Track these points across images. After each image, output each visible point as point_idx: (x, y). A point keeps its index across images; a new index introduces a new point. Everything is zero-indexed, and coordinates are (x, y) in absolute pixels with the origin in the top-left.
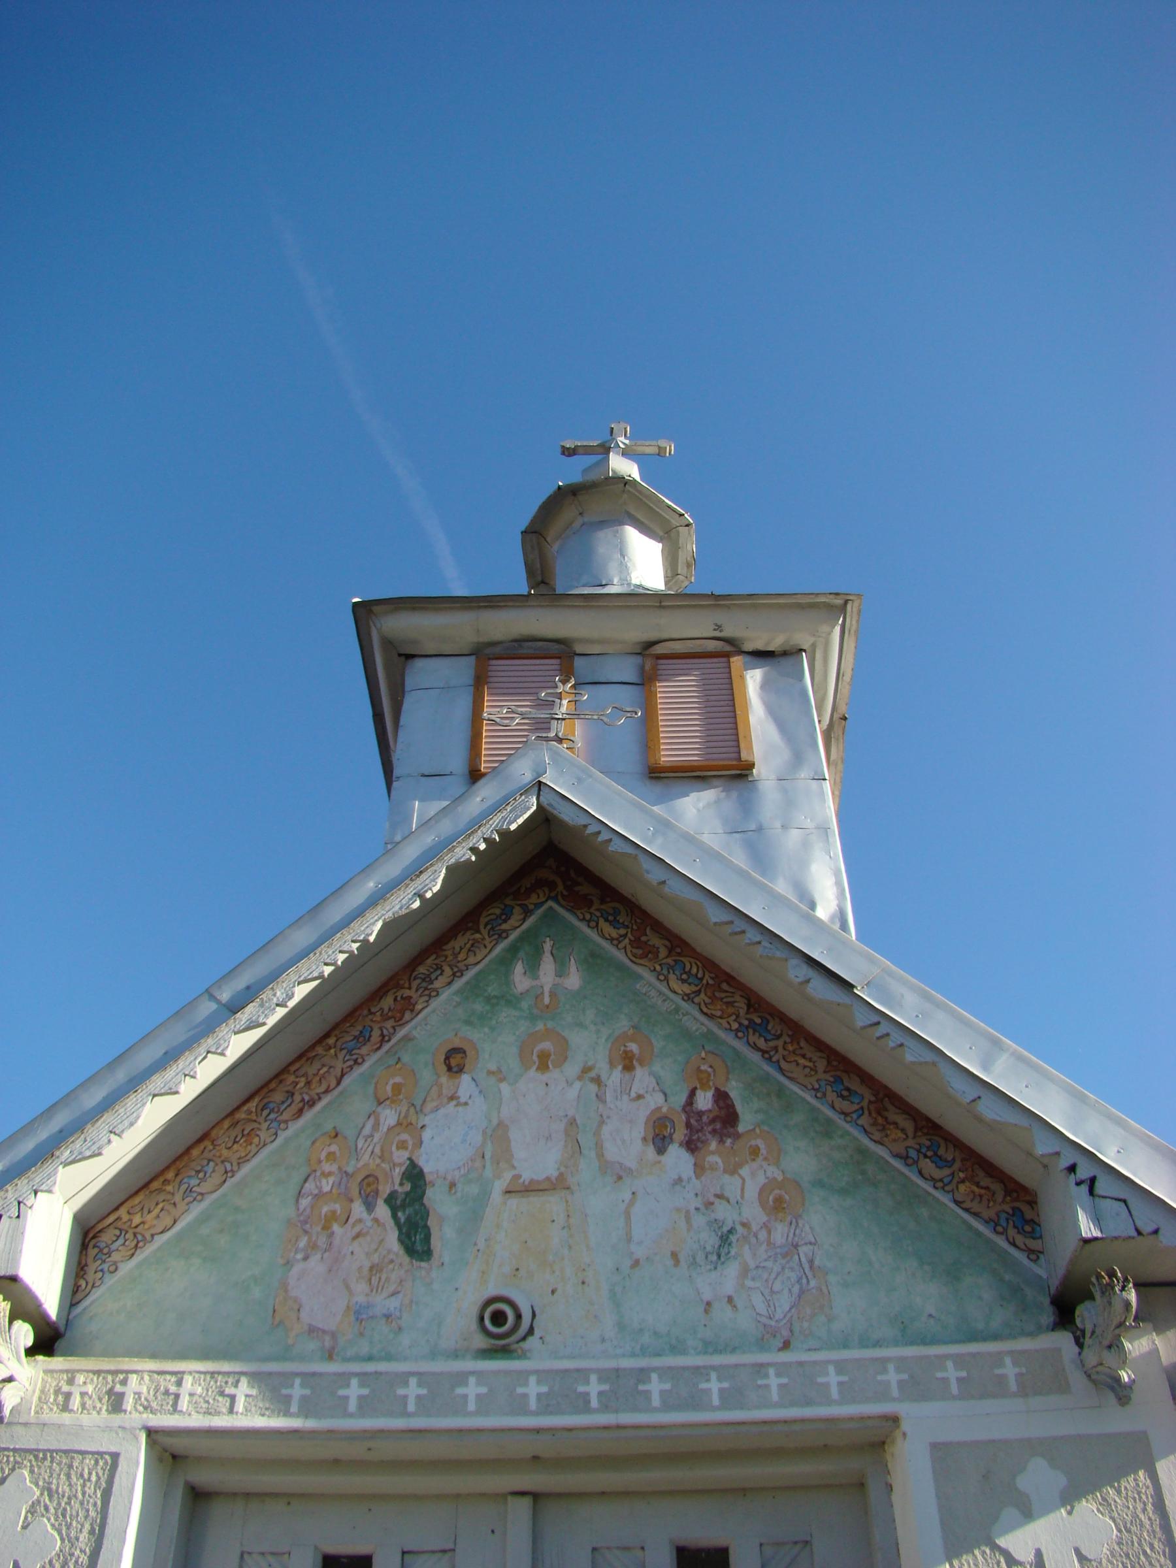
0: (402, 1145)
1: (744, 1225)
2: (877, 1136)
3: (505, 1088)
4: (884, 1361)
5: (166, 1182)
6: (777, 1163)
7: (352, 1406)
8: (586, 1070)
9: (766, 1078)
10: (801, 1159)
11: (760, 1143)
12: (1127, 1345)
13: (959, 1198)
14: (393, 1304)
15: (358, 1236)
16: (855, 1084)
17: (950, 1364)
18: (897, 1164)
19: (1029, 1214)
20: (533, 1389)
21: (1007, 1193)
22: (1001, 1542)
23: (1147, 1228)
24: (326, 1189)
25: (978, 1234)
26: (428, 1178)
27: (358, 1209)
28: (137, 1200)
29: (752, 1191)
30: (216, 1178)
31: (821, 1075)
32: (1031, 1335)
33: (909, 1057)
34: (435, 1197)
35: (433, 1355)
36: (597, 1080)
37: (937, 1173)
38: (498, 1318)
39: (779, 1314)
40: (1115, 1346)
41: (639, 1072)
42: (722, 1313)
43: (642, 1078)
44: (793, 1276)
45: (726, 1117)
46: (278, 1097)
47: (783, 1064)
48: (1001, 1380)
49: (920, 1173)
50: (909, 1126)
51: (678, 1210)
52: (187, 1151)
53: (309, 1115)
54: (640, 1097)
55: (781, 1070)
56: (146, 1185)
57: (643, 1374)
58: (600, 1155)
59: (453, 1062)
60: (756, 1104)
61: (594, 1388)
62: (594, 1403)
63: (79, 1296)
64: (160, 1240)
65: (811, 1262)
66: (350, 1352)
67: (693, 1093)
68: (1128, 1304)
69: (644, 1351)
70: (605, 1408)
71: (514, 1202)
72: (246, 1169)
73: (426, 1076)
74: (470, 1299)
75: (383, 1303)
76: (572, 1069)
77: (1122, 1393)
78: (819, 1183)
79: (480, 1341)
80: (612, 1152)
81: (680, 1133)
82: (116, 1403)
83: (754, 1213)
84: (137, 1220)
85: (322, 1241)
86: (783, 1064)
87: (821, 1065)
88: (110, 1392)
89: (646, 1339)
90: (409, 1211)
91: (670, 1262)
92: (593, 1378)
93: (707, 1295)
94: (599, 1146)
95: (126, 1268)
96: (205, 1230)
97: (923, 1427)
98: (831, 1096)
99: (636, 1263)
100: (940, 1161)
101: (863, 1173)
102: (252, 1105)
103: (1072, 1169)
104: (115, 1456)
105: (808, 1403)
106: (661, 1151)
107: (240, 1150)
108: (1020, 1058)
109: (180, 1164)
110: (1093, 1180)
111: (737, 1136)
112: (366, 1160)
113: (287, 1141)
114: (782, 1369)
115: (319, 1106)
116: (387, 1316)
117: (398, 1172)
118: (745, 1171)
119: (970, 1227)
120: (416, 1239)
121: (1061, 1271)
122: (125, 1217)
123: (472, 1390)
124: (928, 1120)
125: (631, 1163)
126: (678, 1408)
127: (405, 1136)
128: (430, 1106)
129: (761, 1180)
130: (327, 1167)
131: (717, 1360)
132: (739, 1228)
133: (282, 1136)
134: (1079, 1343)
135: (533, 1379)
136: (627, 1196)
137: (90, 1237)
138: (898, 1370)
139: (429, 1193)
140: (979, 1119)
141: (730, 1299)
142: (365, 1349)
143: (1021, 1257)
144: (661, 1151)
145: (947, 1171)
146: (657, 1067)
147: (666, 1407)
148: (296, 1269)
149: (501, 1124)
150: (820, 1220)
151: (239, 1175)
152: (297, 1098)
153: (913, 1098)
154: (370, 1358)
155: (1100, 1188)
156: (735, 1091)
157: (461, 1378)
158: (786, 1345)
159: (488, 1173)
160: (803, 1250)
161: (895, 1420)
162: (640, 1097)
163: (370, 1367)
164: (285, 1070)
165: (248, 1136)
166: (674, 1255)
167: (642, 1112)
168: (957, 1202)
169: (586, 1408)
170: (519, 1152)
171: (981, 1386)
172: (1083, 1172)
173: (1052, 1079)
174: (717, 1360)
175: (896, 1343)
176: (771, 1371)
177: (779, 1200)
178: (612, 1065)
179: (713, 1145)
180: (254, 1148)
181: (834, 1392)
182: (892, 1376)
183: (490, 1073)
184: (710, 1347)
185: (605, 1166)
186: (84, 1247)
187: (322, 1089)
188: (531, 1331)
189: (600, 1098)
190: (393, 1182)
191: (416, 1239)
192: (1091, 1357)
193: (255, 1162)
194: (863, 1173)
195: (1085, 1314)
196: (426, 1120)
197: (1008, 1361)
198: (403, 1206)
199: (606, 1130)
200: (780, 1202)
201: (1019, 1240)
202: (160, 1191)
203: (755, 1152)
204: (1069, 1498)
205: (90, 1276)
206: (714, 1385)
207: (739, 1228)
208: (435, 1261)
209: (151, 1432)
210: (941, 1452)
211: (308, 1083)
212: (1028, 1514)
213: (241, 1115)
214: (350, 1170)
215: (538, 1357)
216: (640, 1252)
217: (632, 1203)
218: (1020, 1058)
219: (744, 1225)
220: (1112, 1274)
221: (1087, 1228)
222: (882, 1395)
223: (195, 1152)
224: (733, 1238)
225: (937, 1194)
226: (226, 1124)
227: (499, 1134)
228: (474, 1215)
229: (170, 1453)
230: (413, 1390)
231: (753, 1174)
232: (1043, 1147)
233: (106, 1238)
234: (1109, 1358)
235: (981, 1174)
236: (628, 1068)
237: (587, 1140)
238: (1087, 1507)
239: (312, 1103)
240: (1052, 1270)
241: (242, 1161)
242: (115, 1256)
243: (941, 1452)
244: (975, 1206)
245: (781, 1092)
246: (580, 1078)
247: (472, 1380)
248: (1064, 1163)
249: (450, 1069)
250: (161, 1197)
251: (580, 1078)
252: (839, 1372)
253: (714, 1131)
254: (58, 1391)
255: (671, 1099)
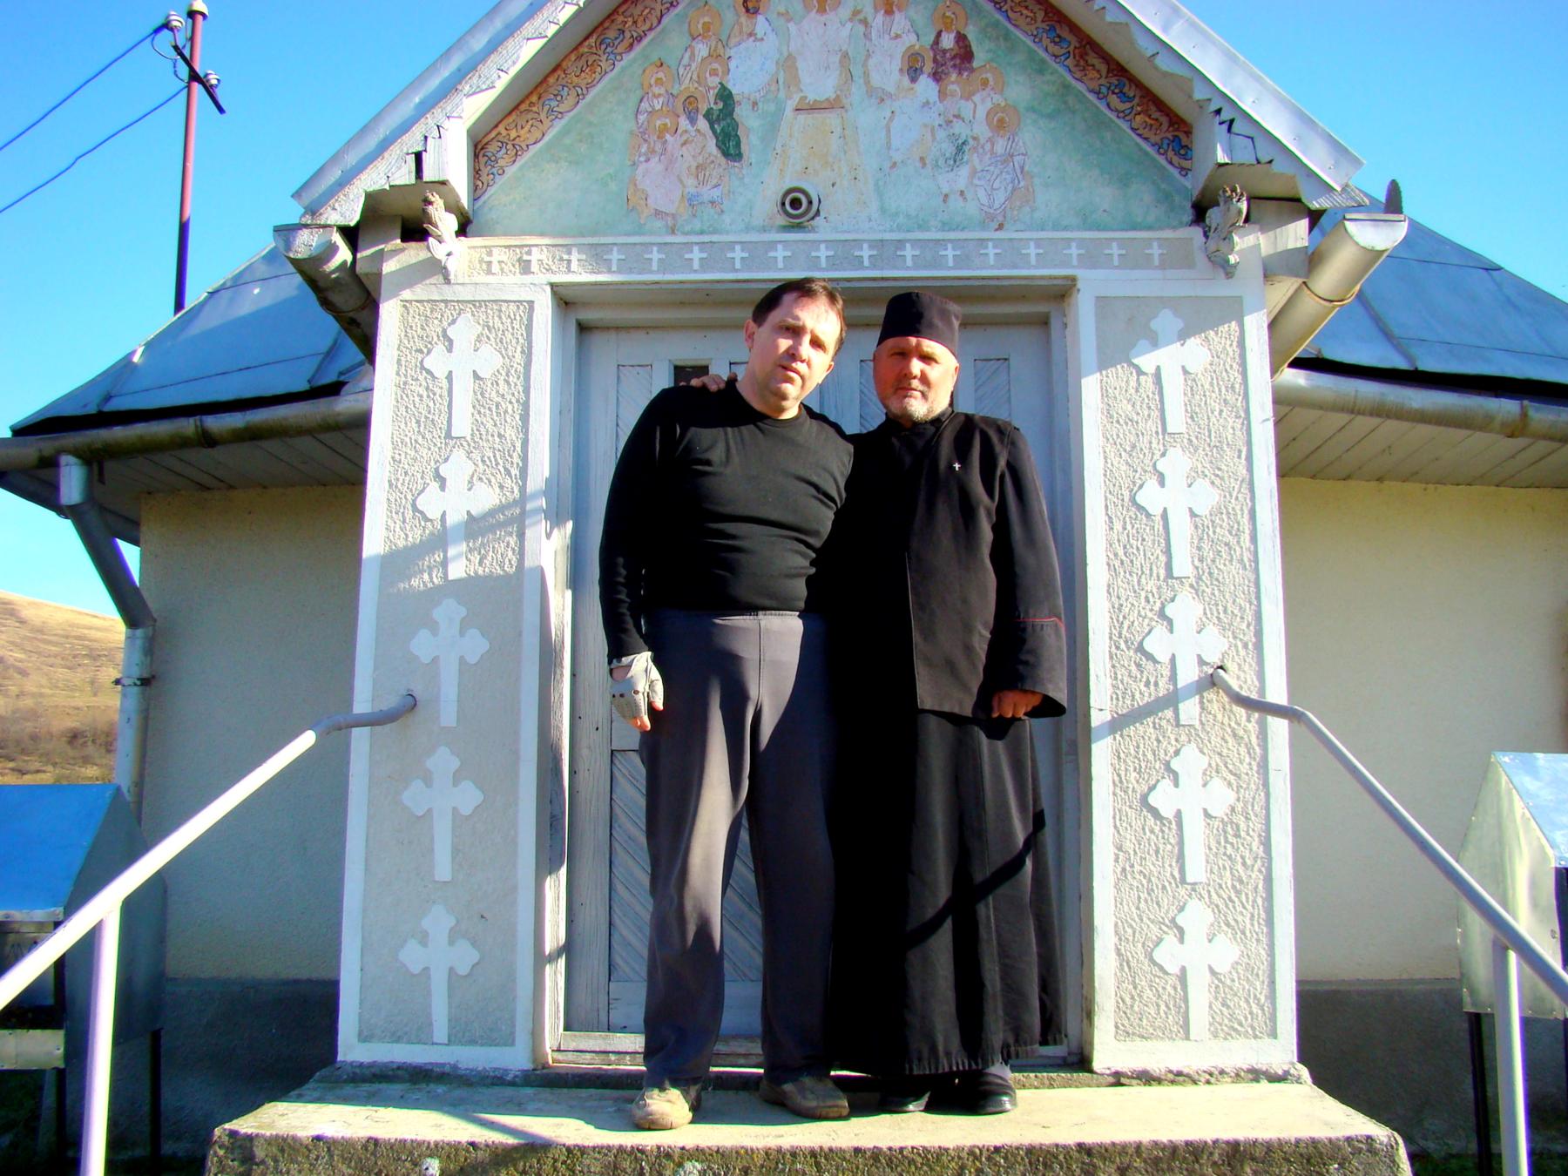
0: (714, 73)
1: (975, 139)
2: (1078, 75)
3: (791, 26)
4: (1070, 240)
5: (532, 104)
6: (1001, 92)
7: (696, 265)
8: (856, 13)
9: (996, 25)
10: (1019, 90)
11: (989, 76)
12: (1236, 238)
13: (1135, 125)
14: (716, 193)
15: (684, 144)
16: (1065, 33)
17: (1114, 245)
18: (1092, 97)
19: (1185, 141)
20: (823, 253)
21: (1171, 124)
22: (1135, 361)
23: (1264, 159)
24: (658, 107)
25: (1146, 154)
26: (736, 98)
27: (684, 123)
28: (510, 119)
29: (981, 113)
30: (571, 100)
31: (1039, 24)
32: (1174, 228)
33: (1109, 19)
34: (742, 113)
35: (748, 229)
36: (865, 22)
37: (1122, 107)
38: (796, 203)
39: (997, 205)
40: (1227, 238)
41: (898, 16)
42: (956, 203)
43: (900, 21)
44: (1009, 177)
45: (964, 55)
46: (611, 34)
47: (1010, 14)
48: (1149, 257)
49: (1108, 105)
50: (1103, 68)
51: (926, 126)
52: (545, 80)
53: (638, 49)
54: (897, 36)
55: (1009, 19)
56: (516, 107)
57: (900, 243)
58: (867, 82)
59: (750, 5)
60: (988, 45)
61: (866, 253)
62: (866, 263)
63: (479, 192)
64: (534, 149)
65: (1022, 168)
66: (687, 228)
67: (939, 34)
68: (1240, 212)
69: (899, 228)
70: (873, 266)
71: (802, 117)
72: (594, 92)
73: (729, 17)
74: (773, 188)
75: (708, 193)
76: (844, 12)
77: (1228, 270)
78: (1031, 109)
79: (782, 220)
80: (876, 80)
81: (929, 67)
82: (525, 267)
83: (982, 130)
84: (513, 134)
85: (658, 147)
86: (1010, 14)
87: (1040, 15)
88: (519, 260)
89: (901, 220)
90: (723, 124)
91: (919, 165)
92: (865, 246)
93: (945, 191)
94: (866, 75)
95: (511, 171)
96: (567, 141)
97: (1092, 286)
98: (1046, 42)
99: (894, 165)
100: (1123, 96)
101: (1065, 103)
102: (592, 41)
103: (1218, 112)
104: (531, 303)
105: (1015, 267)
106: (914, 80)
107: (586, 78)
108: (1193, 25)
109: (541, 90)
110: (1232, 121)
111: (972, 70)
112: (687, 85)
113: (623, 69)
114: (998, 243)
115: (645, 42)
116: (712, 203)
117: (712, 94)
118: (977, 98)
119: (1141, 149)
120: (730, 144)
121: (1201, 186)
122: (504, 133)
123: (780, 253)
124: (1118, 64)
125: (891, 89)
126: (925, 267)
127: (715, 66)
128: (733, 41)
129: (989, 105)
130: (657, 90)
131: (952, 235)
132: (971, 141)
133: (619, 65)
134: (1206, 235)
135: (823, 246)
136: (888, 114)
137: (479, 148)
138: (1078, 248)
139: (737, 110)
140: (1156, 68)
141: (962, 193)
142: (698, 226)
143: (1175, 172)
144: (914, 80)
145: (1128, 105)
146: (912, 12)
147: (916, 267)
148: (642, 168)
149: (790, 56)
150: (1031, 137)
151: (588, 98)
152: (628, 35)
153: (1108, 47)
154: (702, 233)
155: (1235, 128)
156: (972, 34)
157: (772, 245)
158: (1001, 227)
159: (782, 95)
160: (1017, 159)
161: (1073, 279)
162: (897, 36)
163: (706, 239)
164: (615, 11)
165: (592, 66)
166: (922, 159)
167: (899, 49)
168: (1133, 129)
169: (861, 267)
170: (805, 78)
171: (1134, 260)
172: (1225, 116)
173: (1214, 43)
174: (952, 235)
175: (1079, 229)
176: (990, 244)
177: (1001, 121)
178: (876, 9)
179: (954, 77)
180: (597, 76)
181: (1033, 260)
182: (1074, 251)
183: (779, 14)
184: (945, 226)
185: (871, 91)
186: (476, 156)
187: (645, 28)
188: (818, 213)
189: (867, 36)
190: (709, 102)
191: (730, 144)
192: (1212, 245)
193: (600, 86)
194: (1065, 103)
195: (1213, 216)
196: (732, 52)
197: (1155, 245)
198: (718, 120)
199: (871, 62)
200: (1001, 123)
201: (1175, 159)
202: (528, 111)
203: (985, 83)
204: (1183, 336)
205: (484, 178)
206: (950, 253)
207: (971, 141)
208: (745, 161)
209: (552, 285)
210: (1102, 302)
211: (635, 22)
212: (1155, 344)
213: (584, 49)
214: (675, 92)
215: (823, 229)
216: (897, 157)
217: (891, 119)
218: (1193, 25)
219: (975, 139)
220: (1233, 190)
221: (1222, 157)
222: (1065, 263)
223: (551, 80)
224: (966, 148)
225: (1119, 122)
226: (573, 57)
227: (788, 63)
228: (773, 128)
229: (565, 300)
230: (738, 254)
231: (983, 101)
232: (1199, 94)
233: (492, 148)
234: (1223, 246)
235: (1153, 108)
236: (889, 12)
237: (857, 71)
238: (1193, 342)
239: (639, 39)
240: (1193, 185)
241: (590, 86)
242: (501, 163)
243: (1102, 302)
244: (1146, 133)
245: (1007, 36)
246: (851, 20)
247: (780, 247)
248: (1213, 107)
249: (747, 11)
250: (530, 116)
251: (851, 20)
252: (1038, 246)
253: (954, 66)
254: (481, 261)
255: (922, 39)
